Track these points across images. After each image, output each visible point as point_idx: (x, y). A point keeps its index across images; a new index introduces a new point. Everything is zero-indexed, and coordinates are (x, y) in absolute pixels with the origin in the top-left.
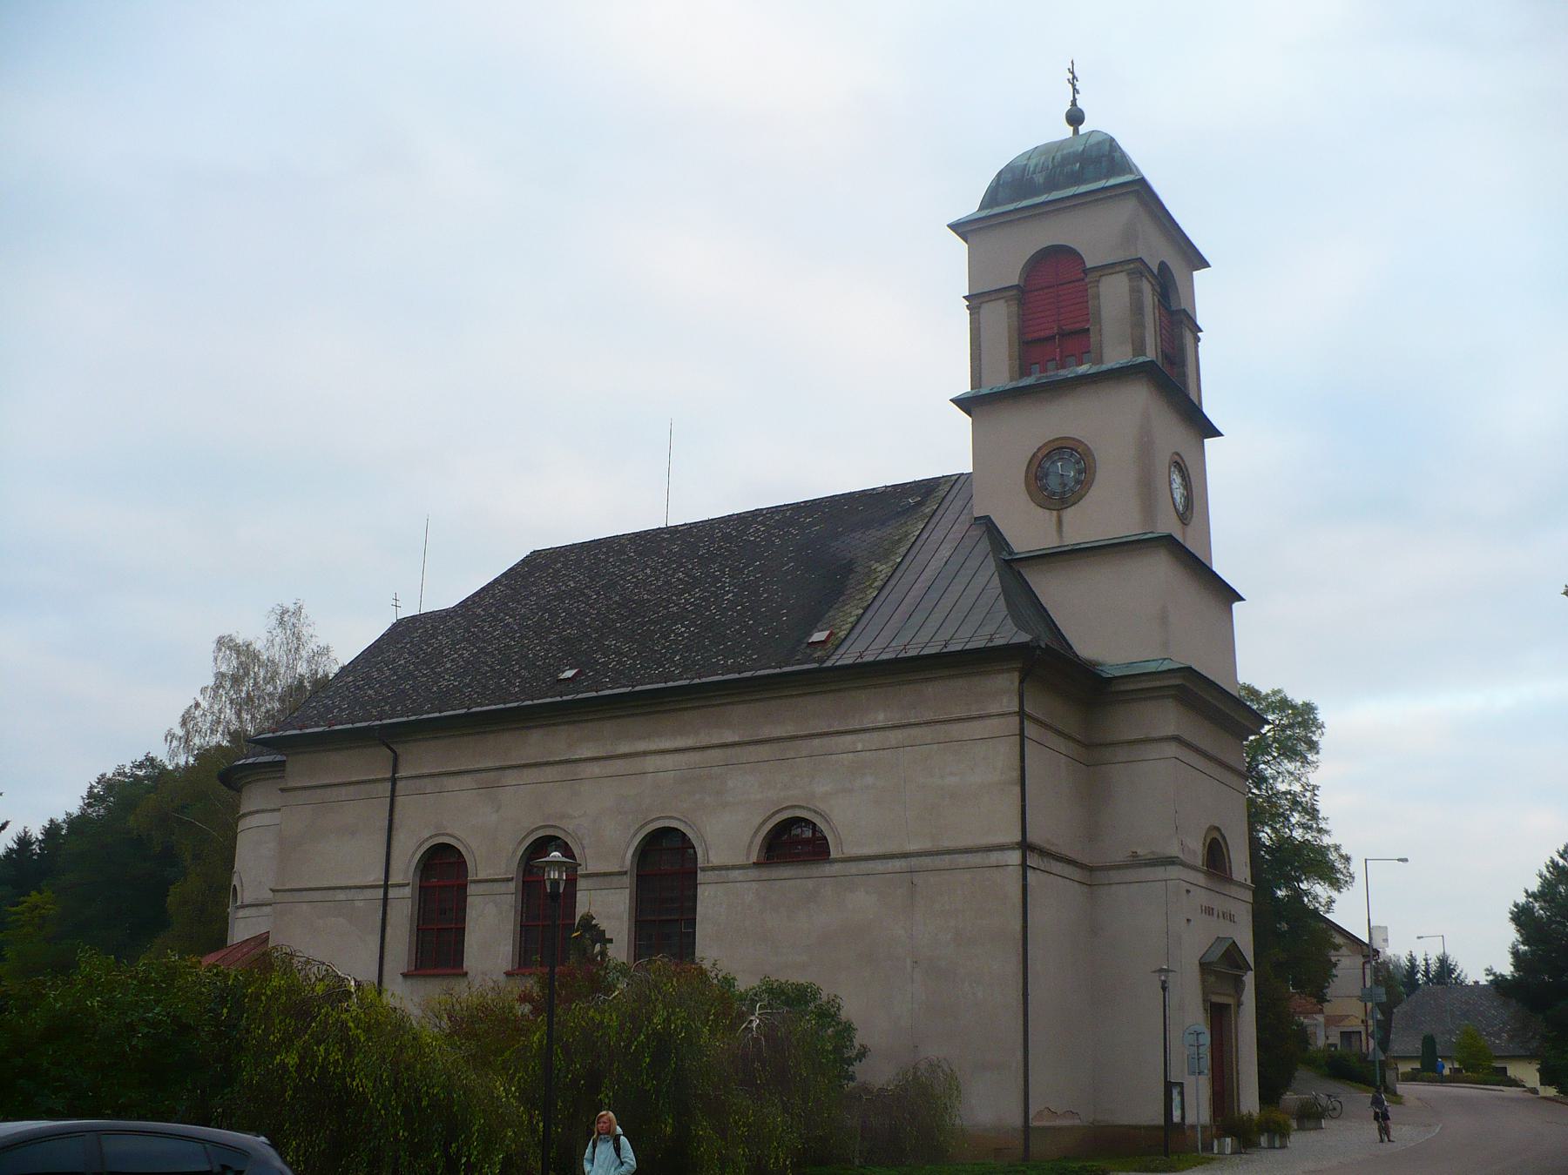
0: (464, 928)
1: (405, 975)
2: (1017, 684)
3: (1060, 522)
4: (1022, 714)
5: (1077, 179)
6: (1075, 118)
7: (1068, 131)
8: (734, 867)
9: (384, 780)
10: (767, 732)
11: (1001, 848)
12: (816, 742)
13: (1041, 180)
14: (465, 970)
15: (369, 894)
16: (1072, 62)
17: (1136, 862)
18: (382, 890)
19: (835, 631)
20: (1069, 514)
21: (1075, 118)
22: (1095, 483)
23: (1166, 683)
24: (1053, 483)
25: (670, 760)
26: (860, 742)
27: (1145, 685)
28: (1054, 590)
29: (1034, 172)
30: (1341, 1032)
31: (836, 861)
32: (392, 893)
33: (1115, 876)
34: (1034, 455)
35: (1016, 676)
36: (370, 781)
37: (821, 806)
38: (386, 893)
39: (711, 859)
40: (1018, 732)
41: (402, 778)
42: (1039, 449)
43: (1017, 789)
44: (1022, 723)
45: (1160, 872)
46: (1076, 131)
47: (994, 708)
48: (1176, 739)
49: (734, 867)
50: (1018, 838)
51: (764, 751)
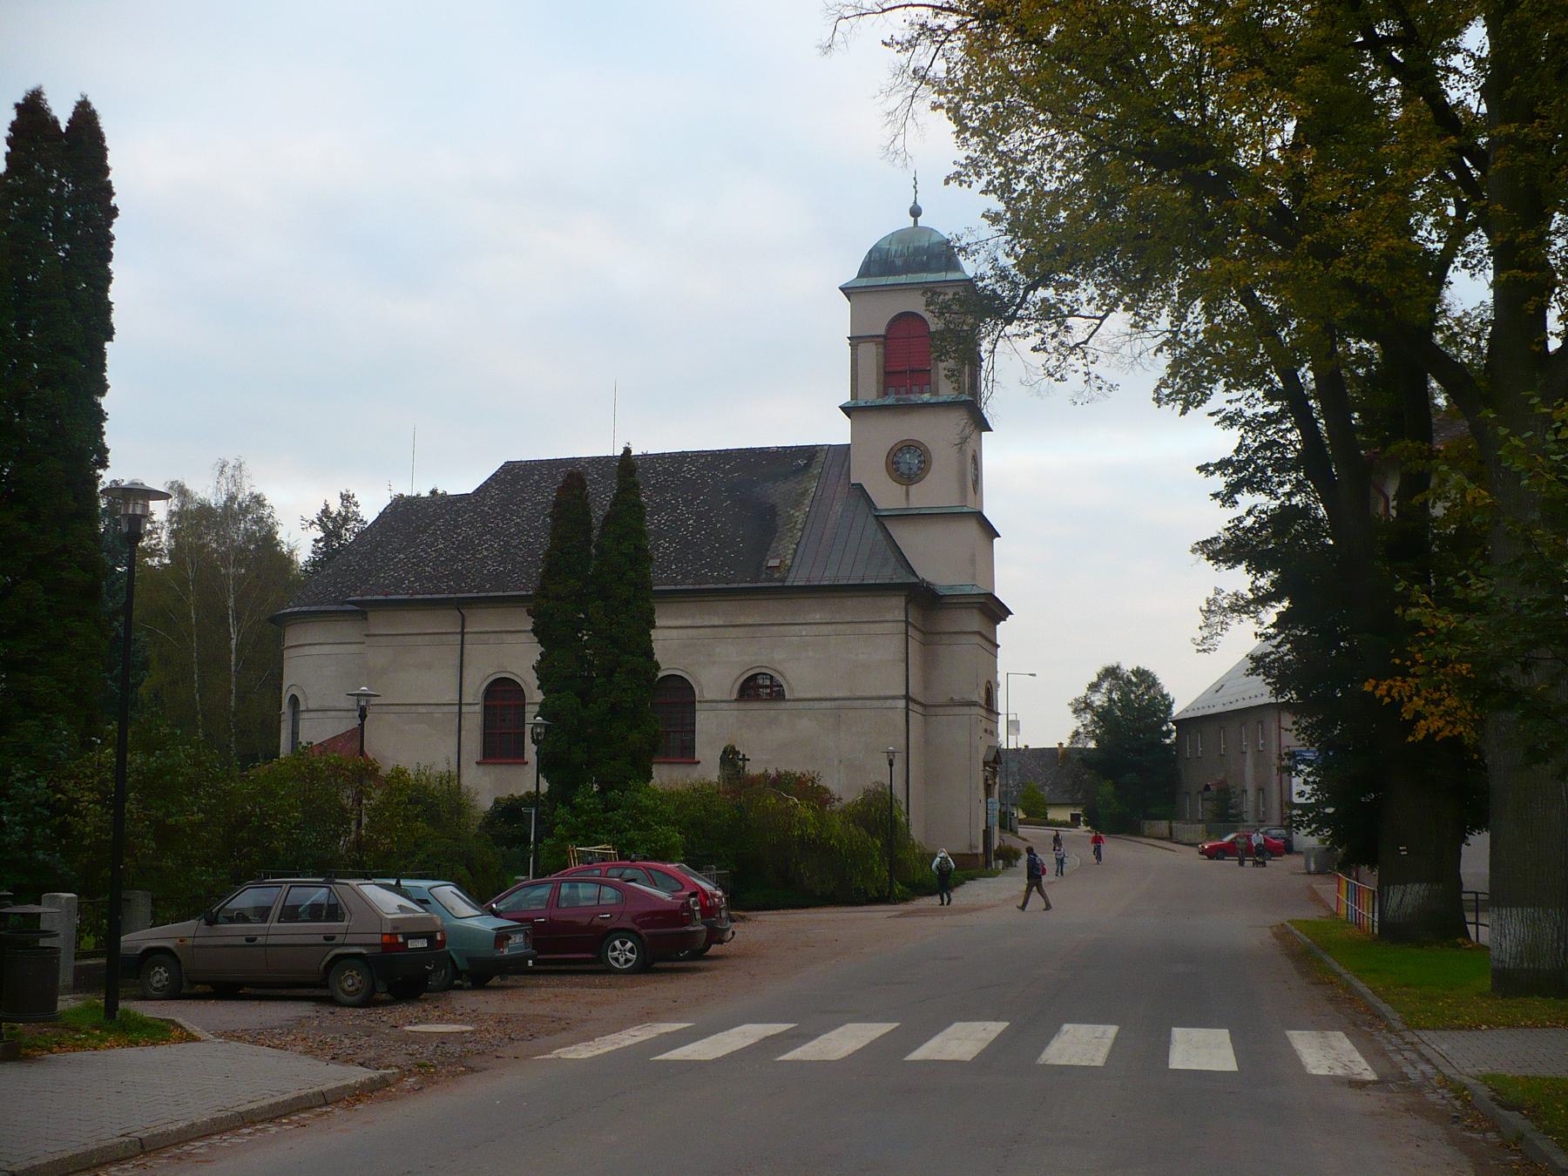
0: (524, 733)
1: (477, 763)
2: (903, 604)
4: (907, 622)
5: (925, 268)
6: (915, 212)
8: (722, 701)
9: (457, 633)
10: (742, 620)
12: (775, 628)
13: (900, 263)
14: (526, 760)
15: (446, 709)
16: (1223, 686)
17: (953, 703)
18: (457, 707)
19: (783, 559)
20: (913, 489)
21: (915, 212)
22: (931, 471)
23: (977, 600)
24: (903, 468)
25: (675, 633)
26: (804, 630)
27: (963, 601)
29: (895, 256)
31: (789, 700)
32: (464, 709)
34: (892, 448)
35: (903, 599)
36: (442, 633)
37: (779, 668)
38: (460, 709)
39: (705, 695)
40: (904, 632)
41: (467, 633)
42: (896, 444)
43: (904, 665)
44: (907, 627)
45: (966, 710)
46: (916, 222)
47: (889, 617)
48: (979, 633)
49: (722, 701)
50: (904, 693)
51: (740, 632)
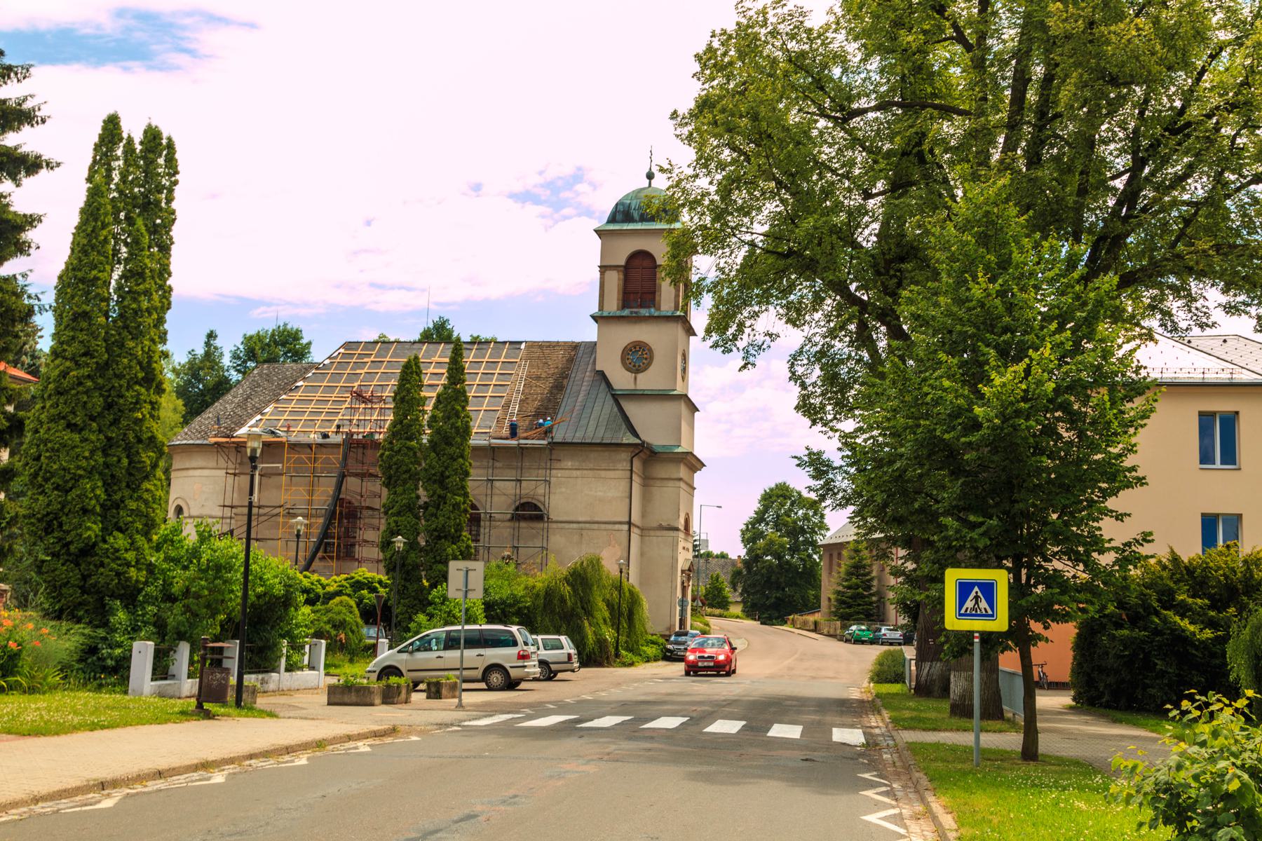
3: (635, 378)
7: (645, 183)
11: (620, 523)
20: (640, 376)
28: (631, 409)
30: (1200, 412)
33: (652, 533)
43: (628, 500)
50: (627, 520)
